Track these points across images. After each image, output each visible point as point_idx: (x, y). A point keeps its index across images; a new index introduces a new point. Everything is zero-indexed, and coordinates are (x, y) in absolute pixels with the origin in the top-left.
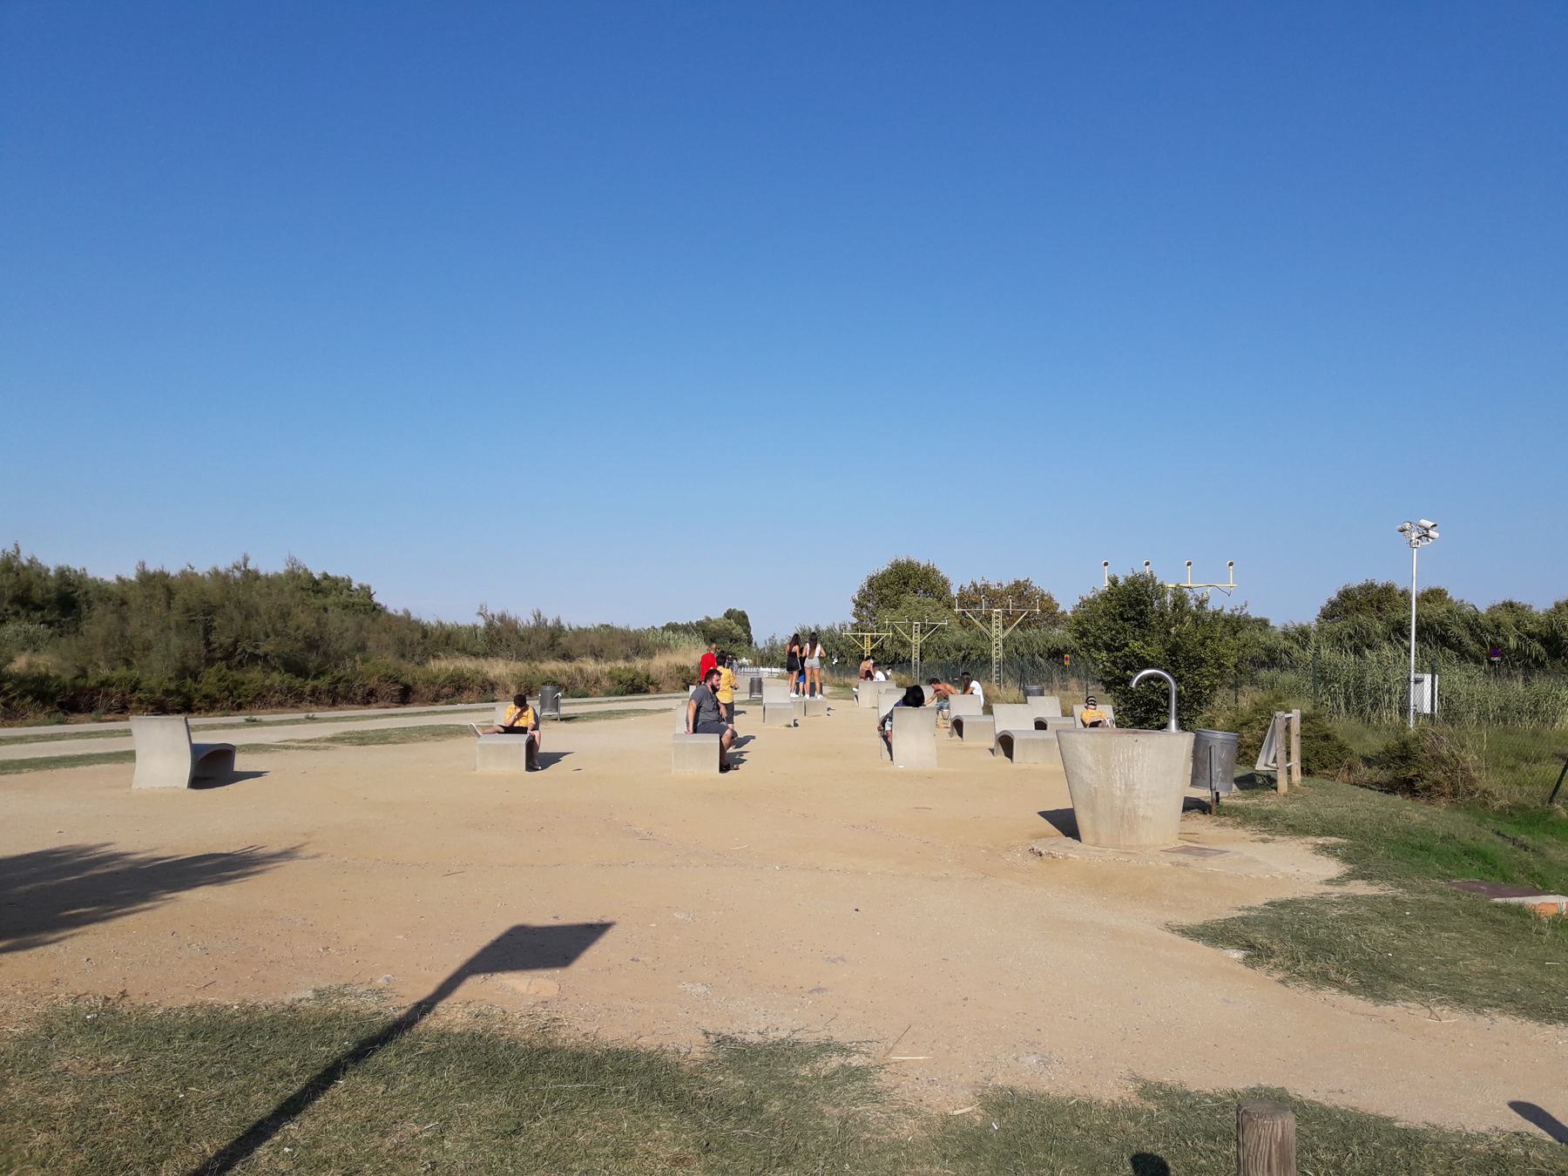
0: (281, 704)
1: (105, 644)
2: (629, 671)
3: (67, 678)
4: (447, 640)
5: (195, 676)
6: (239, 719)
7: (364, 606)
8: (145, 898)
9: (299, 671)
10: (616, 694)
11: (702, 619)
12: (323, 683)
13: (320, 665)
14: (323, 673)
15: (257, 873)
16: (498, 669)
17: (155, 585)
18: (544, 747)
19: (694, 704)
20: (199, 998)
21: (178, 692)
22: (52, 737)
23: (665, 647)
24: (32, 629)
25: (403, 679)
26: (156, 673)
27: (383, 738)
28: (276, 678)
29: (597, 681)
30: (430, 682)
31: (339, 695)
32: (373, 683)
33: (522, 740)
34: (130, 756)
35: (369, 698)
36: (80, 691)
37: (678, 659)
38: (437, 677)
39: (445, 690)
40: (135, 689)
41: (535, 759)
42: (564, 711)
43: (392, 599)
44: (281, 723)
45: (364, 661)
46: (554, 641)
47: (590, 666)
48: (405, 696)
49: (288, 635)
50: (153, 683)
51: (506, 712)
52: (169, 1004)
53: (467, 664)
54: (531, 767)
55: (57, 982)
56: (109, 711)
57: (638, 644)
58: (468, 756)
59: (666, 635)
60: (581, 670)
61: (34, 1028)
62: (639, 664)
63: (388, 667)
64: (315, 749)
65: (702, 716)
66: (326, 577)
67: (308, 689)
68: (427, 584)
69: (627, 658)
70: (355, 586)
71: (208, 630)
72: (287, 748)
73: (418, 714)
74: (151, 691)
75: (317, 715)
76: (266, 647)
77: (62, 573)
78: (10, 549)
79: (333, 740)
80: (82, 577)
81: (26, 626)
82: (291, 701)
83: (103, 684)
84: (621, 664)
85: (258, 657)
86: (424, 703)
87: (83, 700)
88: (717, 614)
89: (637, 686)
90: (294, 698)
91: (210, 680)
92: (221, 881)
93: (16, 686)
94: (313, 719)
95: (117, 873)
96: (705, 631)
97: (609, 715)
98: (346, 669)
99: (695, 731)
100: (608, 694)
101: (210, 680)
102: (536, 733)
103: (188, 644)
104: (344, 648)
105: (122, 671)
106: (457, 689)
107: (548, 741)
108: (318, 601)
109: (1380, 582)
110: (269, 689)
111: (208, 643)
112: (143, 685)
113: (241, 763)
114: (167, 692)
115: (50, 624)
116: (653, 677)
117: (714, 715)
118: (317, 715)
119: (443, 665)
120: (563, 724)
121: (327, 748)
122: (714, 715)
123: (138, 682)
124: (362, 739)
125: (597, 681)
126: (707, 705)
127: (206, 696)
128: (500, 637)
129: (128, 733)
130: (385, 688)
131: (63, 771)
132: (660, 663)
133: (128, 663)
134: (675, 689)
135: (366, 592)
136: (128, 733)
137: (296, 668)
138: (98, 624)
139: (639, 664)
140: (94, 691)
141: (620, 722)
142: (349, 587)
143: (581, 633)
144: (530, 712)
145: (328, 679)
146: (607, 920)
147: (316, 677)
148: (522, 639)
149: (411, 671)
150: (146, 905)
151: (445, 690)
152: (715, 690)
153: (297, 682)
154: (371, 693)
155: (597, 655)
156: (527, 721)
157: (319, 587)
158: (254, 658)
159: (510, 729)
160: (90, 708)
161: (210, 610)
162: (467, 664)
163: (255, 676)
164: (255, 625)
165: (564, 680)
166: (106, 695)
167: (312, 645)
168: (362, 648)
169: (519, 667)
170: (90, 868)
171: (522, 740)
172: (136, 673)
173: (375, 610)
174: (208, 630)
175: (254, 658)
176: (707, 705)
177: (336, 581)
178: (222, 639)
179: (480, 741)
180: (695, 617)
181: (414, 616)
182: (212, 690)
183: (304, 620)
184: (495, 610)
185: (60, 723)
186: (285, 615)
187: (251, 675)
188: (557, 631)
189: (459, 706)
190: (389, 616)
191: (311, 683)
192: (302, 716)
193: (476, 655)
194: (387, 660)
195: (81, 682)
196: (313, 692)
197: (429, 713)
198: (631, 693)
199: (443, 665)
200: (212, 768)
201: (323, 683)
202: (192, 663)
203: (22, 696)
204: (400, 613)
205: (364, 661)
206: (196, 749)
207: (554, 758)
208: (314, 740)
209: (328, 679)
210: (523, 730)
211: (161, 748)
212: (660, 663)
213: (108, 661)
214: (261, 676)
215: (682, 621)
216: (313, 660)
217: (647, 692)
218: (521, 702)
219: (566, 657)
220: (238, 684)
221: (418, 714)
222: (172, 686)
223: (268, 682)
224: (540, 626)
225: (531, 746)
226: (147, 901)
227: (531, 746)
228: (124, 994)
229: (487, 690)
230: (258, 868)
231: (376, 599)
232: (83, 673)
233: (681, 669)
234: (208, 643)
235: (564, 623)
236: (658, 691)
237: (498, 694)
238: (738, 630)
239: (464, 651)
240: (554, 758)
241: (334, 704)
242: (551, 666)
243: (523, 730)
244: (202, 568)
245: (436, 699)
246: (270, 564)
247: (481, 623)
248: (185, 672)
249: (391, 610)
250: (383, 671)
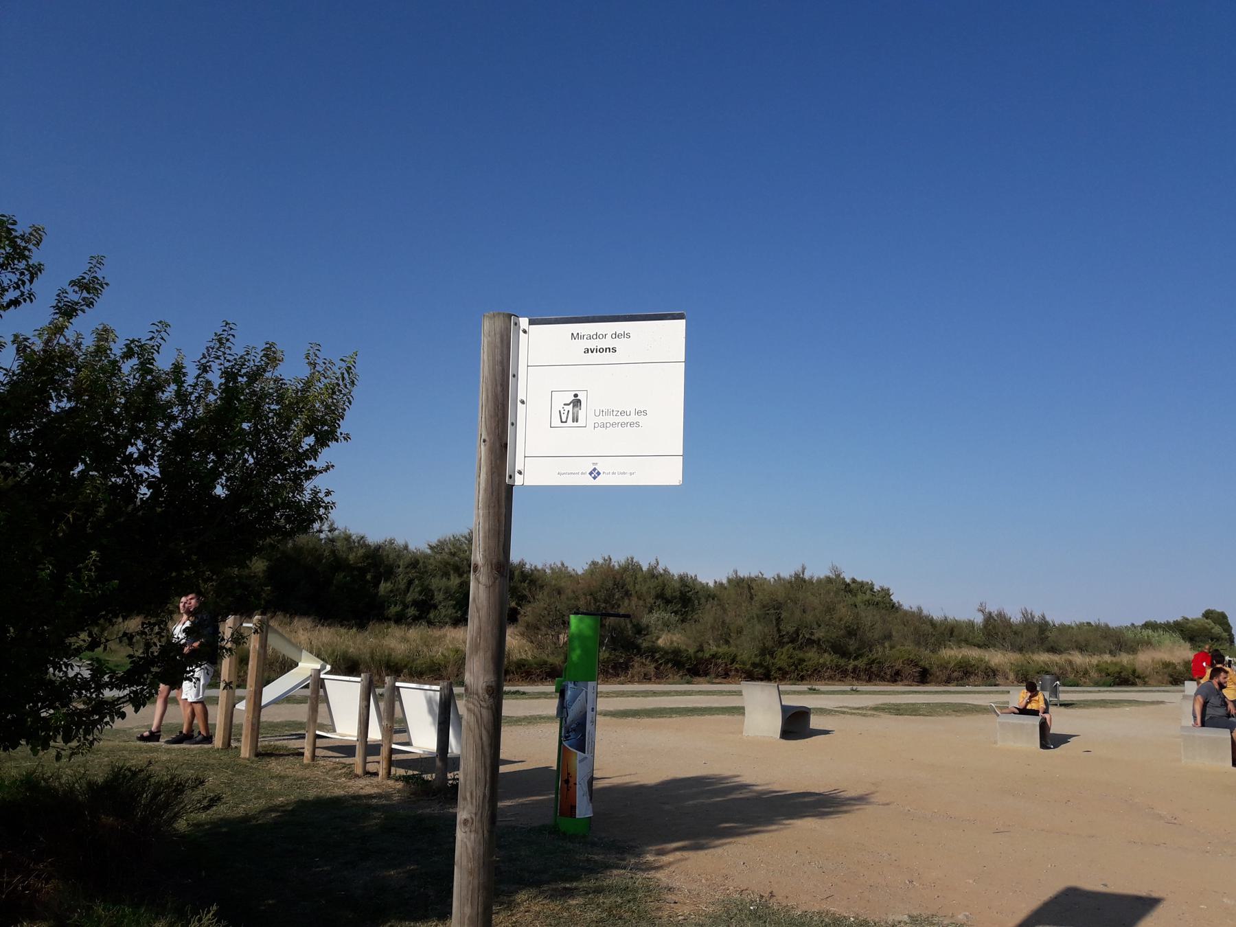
0: (831, 678)
1: (713, 628)
2: (1116, 664)
3: (691, 651)
4: (951, 632)
5: (772, 654)
6: (803, 687)
7: (882, 602)
8: (770, 821)
9: (842, 652)
10: (1104, 685)
11: (1179, 619)
12: (861, 663)
13: (859, 649)
14: (861, 655)
15: (846, 812)
16: (996, 658)
17: (744, 587)
18: (1054, 729)
19: (1200, 699)
20: (824, 907)
21: (760, 665)
22: (678, 693)
23: (1148, 643)
24: (667, 616)
25: (922, 663)
26: (747, 651)
27: (913, 710)
28: (827, 658)
29: (1086, 673)
30: (944, 666)
31: (875, 673)
32: (898, 665)
33: (1035, 721)
34: (740, 711)
35: (896, 677)
36: (701, 661)
37: (1163, 655)
38: (949, 663)
39: (955, 674)
40: (733, 661)
41: (1048, 739)
42: (1063, 697)
43: (905, 598)
44: (833, 692)
45: (892, 647)
46: (1039, 635)
47: (1078, 659)
48: (924, 677)
49: (833, 625)
50: (745, 657)
51: (1019, 696)
52: (805, 908)
53: (973, 653)
54: (1044, 746)
55: (726, 877)
56: (717, 676)
57: (1117, 640)
58: (984, 734)
59: (1145, 633)
60: (1071, 662)
61: (719, 909)
62: (1125, 659)
63: (910, 653)
64: (864, 715)
65: (1209, 711)
66: (854, 581)
67: (850, 667)
68: (935, 583)
69: (1111, 653)
70: (877, 588)
71: (779, 620)
72: (844, 713)
73: (936, 692)
74: (744, 663)
75: (860, 688)
76: (819, 634)
77: (683, 579)
78: (653, 562)
79: (876, 709)
80: (695, 580)
81: (663, 614)
82: (838, 676)
83: (713, 656)
84: (1107, 658)
85: (814, 641)
86: (939, 683)
87: (702, 667)
88: (1194, 613)
89: (1125, 679)
90: (841, 674)
91: (782, 658)
92: (822, 815)
93: (662, 656)
94: (856, 691)
95: (748, 799)
96: (1185, 631)
97: (1103, 703)
98: (878, 652)
99: (1203, 724)
100: (1097, 684)
101: (782, 658)
102: (1047, 716)
103: (766, 630)
104: (876, 637)
105: (724, 649)
106: (964, 674)
107: (1059, 722)
108: (850, 599)
109: (618, 559)
110: (823, 665)
111: (779, 631)
112: (738, 658)
113: (815, 722)
114: (754, 665)
115: (676, 613)
116: (1139, 671)
117: (1222, 711)
118: (860, 688)
119: (952, 653)
120: (1062, 709)
121: (873, 715)
122: (1222, 711)
123: (735, 656)
124: (897, 710)
125: (1086, 673)
126: (1214, 700)
127: (780, 669)
128: (995, 631)
129: (739, 693)
130: (908, 670)
131: (696, 718)
132: (1144, 659)
133: (727, 642)
134: (1161, 683)
135: (886, 593)
136: (739, 693)
137: (839, 649)
138: (708, 615)
139: (1125, 659)
140: (709, 661)
141: (1116, 710)
142: (872, 589)
143: (1063, 629)
144: (1040, 697)
145: (865, 660)
146: (1155, 895)
147: (856, 658)
148: (1015, 633)
149: (926, 656)
150: (774, 827)
151: (955, 674)
152: (1222, 686)
153: (842, 662)
154: (898, 673)
155: (1082, 649)
156: (1038, 704)
157: (852, 589)
158: (810, 642)
159: (1024, 711)
160: (706, 674)
161: (779, 606)
162: (973, 653)
163: (812, 654)
164: (809, 617)
165: (1056, 670)
166: (716, 664)
167: (851, 633)
168: (889, 637)
169: (1014, 657)
170: (730, 793)
171: (1035, 721)
172: (733, 649)
173: (894, 608)
174: (779, 620)
175: (810, 642)
176: (1214, 700)
177: (862, 584)
178: (788, 628)
179: (999, 720)
180: (1173, 617)
181: (925, 612)
182: (784, 665)
183: (843, 611)
184: (993, 608)
185: (688, 683)
186: (830, 610)
187: (810, 655)
188: (1044, 626)
189: (967, 688)
190: (906, 613)
191: (852, 663)
192: (848, 688)
193: (979, 646)
194: (908, 648)
195: (700, 655)
196: (855, 668)
197: (945, 692)
198: (1119, 684)
199: (952, 653)
200: (796, 724)
201: (861, 663)
202: (769, 644)
203: (666, 663)
204: (915, 609)
205: (892, 647)
206: (785, 709)
207: (1062, 739)
208: (862, 708)
209: (865, 660)
210: (1035, 713)
211: (762, 706)
212: (1144, 659)
213: (715, 640)
214: (816, 656)
215: (1161, 620)
216: (852, 645)
217: (1134, 684)
218: (1032, 689)
219: (1053, 650)
220: (802, 660)
221: (936, 692)
222: (757, 660)
223: (821, 661)
224: (1028, 622)
225: (1044, 727)
226: (773, 824)
227: (1044, 727)
228: (772, 895)
229: (990, 676)
230: (845, 808)
231: (895, 599)
232: (701, 649)
233: (1167, 665)
234: (779, 631)
235: (1048, 619)
236: (1145, 684)
237: (999, 680)
238: (1217, 629)
239: (968, 642)
240: (1062, 739)
241: (869, 680)
242: (1043, 658)
243: (1035, 713)
244: (770, 575)
245: (948, 681)
246: (817, 571)
247: (979, 619)
248: (764, 651)
249: (906, 607)
250: (906, 656)
